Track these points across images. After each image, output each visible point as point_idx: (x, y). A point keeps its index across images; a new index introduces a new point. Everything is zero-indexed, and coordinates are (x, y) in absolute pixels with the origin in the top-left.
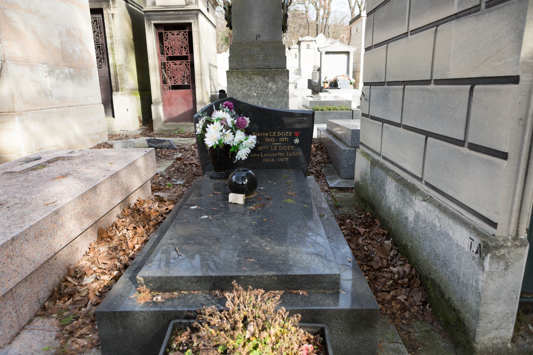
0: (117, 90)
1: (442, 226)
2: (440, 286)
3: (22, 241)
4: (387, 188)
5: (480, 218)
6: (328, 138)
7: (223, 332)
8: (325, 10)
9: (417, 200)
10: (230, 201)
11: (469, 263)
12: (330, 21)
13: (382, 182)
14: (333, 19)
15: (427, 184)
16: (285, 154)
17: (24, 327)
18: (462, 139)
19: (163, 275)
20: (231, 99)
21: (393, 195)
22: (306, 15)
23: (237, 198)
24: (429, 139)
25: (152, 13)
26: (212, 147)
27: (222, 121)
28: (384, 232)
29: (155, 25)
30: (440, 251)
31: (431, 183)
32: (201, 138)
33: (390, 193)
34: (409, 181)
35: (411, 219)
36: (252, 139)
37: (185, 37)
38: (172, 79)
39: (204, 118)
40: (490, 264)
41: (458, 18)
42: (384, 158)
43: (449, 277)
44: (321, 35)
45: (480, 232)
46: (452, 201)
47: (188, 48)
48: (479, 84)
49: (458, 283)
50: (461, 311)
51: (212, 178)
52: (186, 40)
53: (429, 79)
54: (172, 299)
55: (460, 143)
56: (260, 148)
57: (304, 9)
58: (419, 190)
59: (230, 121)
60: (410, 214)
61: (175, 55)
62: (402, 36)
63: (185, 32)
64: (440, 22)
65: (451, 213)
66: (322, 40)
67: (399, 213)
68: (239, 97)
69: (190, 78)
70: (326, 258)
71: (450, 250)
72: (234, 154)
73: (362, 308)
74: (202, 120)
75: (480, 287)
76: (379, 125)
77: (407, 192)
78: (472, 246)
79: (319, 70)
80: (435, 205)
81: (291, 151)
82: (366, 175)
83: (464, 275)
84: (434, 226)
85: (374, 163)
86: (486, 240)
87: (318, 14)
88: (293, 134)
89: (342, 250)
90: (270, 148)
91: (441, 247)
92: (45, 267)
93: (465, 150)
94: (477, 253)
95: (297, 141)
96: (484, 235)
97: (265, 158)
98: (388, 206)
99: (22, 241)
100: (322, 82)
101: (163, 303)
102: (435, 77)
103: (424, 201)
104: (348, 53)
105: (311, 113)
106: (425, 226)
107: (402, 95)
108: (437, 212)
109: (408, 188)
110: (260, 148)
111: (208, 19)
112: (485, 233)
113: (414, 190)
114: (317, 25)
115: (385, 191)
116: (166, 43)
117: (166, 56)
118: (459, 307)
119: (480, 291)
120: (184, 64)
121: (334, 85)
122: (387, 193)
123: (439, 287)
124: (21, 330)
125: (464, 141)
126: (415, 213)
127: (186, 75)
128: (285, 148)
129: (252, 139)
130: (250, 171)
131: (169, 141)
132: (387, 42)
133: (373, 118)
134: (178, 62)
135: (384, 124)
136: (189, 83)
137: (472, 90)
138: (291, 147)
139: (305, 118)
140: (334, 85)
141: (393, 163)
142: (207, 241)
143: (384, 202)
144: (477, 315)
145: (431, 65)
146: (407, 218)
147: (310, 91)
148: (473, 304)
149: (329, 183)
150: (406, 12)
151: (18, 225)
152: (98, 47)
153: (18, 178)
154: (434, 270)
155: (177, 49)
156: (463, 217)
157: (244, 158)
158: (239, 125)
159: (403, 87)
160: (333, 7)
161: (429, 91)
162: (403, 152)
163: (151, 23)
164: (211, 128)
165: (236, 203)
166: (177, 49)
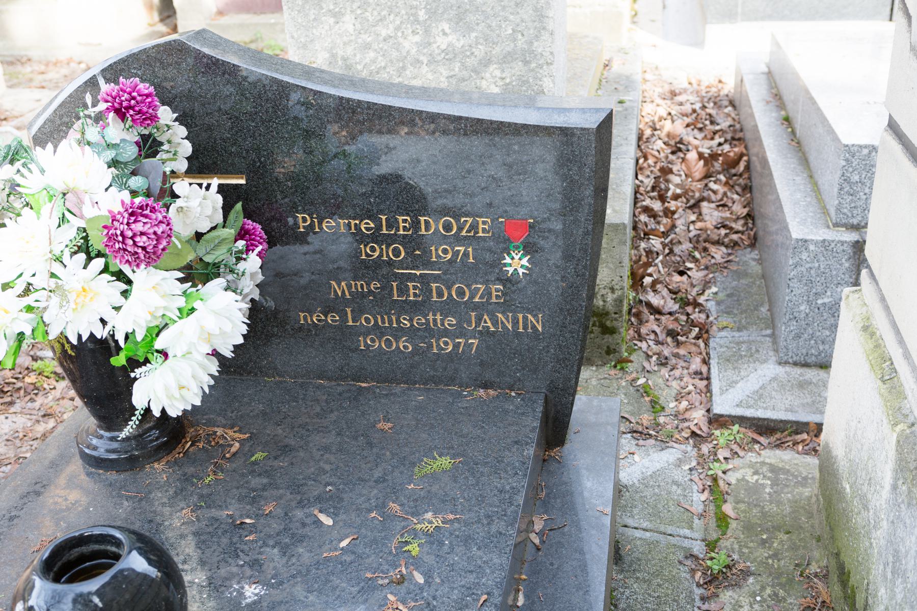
7: (728, 509)
90: (386, 287)
105: (592, 122)
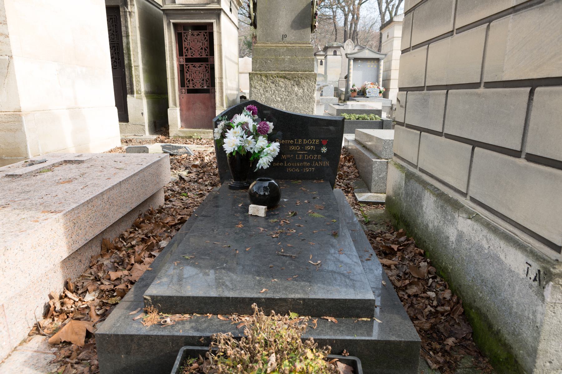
0: (132, 93)
1: (492, 248)
2: (487, 316)
3: (16, 251)
4: (424, 203)
5: (539, 241)
6: (356, 149)
8: (353, 16)
9: (460, 218)
10: (250, 213)
11: (524, 292)
12: (359, 27)
13: (418, 196)
14: (362, 26)
15: (473, 200)
16: (311, 163)
17: (16, 348)
18: (519, 149)
19: (174, 295)
20: (254, 103)
21: (432, 211)
22: (334, 20)
23: (258, 210)
24: (477, 149)
25: (172, 12)
26: (231, 153)
27: (243, 125)
28: (420, 252)
29: (175, 25)
30: (488, 276)
31: (478, 199)
32: (219, 144)
33: (428, 210)
34: (451, 196)
35: (453, 238)
36: (275, 146)
37: (205, 38)
38: (191, 82)
39: (222, 123)
40: (552, 294)
41: (516, 11)
42: (421, 170)
43: (498, 307)
44: (349, 41)
45: (539, 256)
46: (503, 220)
47: (208, 50)
48: (541, 86)
49: (510, 313)
50: (514, 346)
51: (231, 188)
52: (207, 41)
53: (479, 81)
54: (183, 322)
55: (516, 154)
56: (284, 157)
57: (332, 14)
58: (463, 206)
59: (251, 124)
60: (451, 233)
61: (194, 57)
62: (446, 35)
63: (206, 33)
64: (493, 17)
65: (503, 233)
66: (349, 47)
67: (439, 232)
68: (262, 101)
69: (209, 81)
70: (349, 278)
71: (501, 275)
72: (256, 160)
73: (401, 340)
74: (221, 124)
75: (538, 320)
76: (416, 134)
77: (449, 208)
78: (530, 272)
79: (347, 77)
80: (482, 224)
81: (317, 161)
82: (400, 189)
83: (518, 304)
84: (482, 247)
85: (409, 176)
86: (548, 266)
87: (346, 20)
88: (320, 141)
89: (375, 271)
91: (489, 271)
92: (43, 281)
93: (522, 162)
94: (535, 280)
95: (324, 150)
96: (544, 260)
97: (288, 167)
98: (425, 223)
99: (16, 251)
100: (349, 90)
101: (172, 326)
102: (486, 79)
103: (469, 218)
104: (378, 60)
106: (470, 247)
107: (444, 101)
108: (485, 232)
109: (449, 204)
110: (284, 157)
111: (231, 19)
112: (546, 258)
113: (457, 206)
114: (345, 31)
115: (422, 207)
116: (185, 44)
117: (186, 88)
118: (511, 342)
119: (538, 325)
120: (203, 67)
121: (363, 93)
122: (424, 209)
123: (486, 317)
124: (13, 351)
125: (521, 152)
126: (459, 232)
127: (205, 78)
128: (311, 157)
129: (275, 146)
130: (273, 181)
131: (185, 147)
132: (428, 42)
133: (409, 126)
134: (197, 64)
135: (423, 133)
136: (208, 86)
137: (532, 93)
138: (317, 157)
139: (332, 128)
140: (363, 93)
141: (432, 176)
142: (224, 257)
143: (420, 219)
144: (534, 353)
145: (480, 66)
146: (448, 237)
147: (336, 99)
148: (529, 339)
149: (357, 197)
150: (451, 8)
151: (13, 233)
152: (113, 46)
153: (20, 182)
154: (480, 298)
155: (196, 51)
156: (518, 238)
157: (266, 167)
158: (260, 131)
159: (446, 91)
160: (364, 11)
161: (479, 95)
162: (446, 164)
163: (170, 22)
164: (230, 134)
165: (256, 216)
166: (196, 51)
